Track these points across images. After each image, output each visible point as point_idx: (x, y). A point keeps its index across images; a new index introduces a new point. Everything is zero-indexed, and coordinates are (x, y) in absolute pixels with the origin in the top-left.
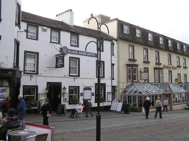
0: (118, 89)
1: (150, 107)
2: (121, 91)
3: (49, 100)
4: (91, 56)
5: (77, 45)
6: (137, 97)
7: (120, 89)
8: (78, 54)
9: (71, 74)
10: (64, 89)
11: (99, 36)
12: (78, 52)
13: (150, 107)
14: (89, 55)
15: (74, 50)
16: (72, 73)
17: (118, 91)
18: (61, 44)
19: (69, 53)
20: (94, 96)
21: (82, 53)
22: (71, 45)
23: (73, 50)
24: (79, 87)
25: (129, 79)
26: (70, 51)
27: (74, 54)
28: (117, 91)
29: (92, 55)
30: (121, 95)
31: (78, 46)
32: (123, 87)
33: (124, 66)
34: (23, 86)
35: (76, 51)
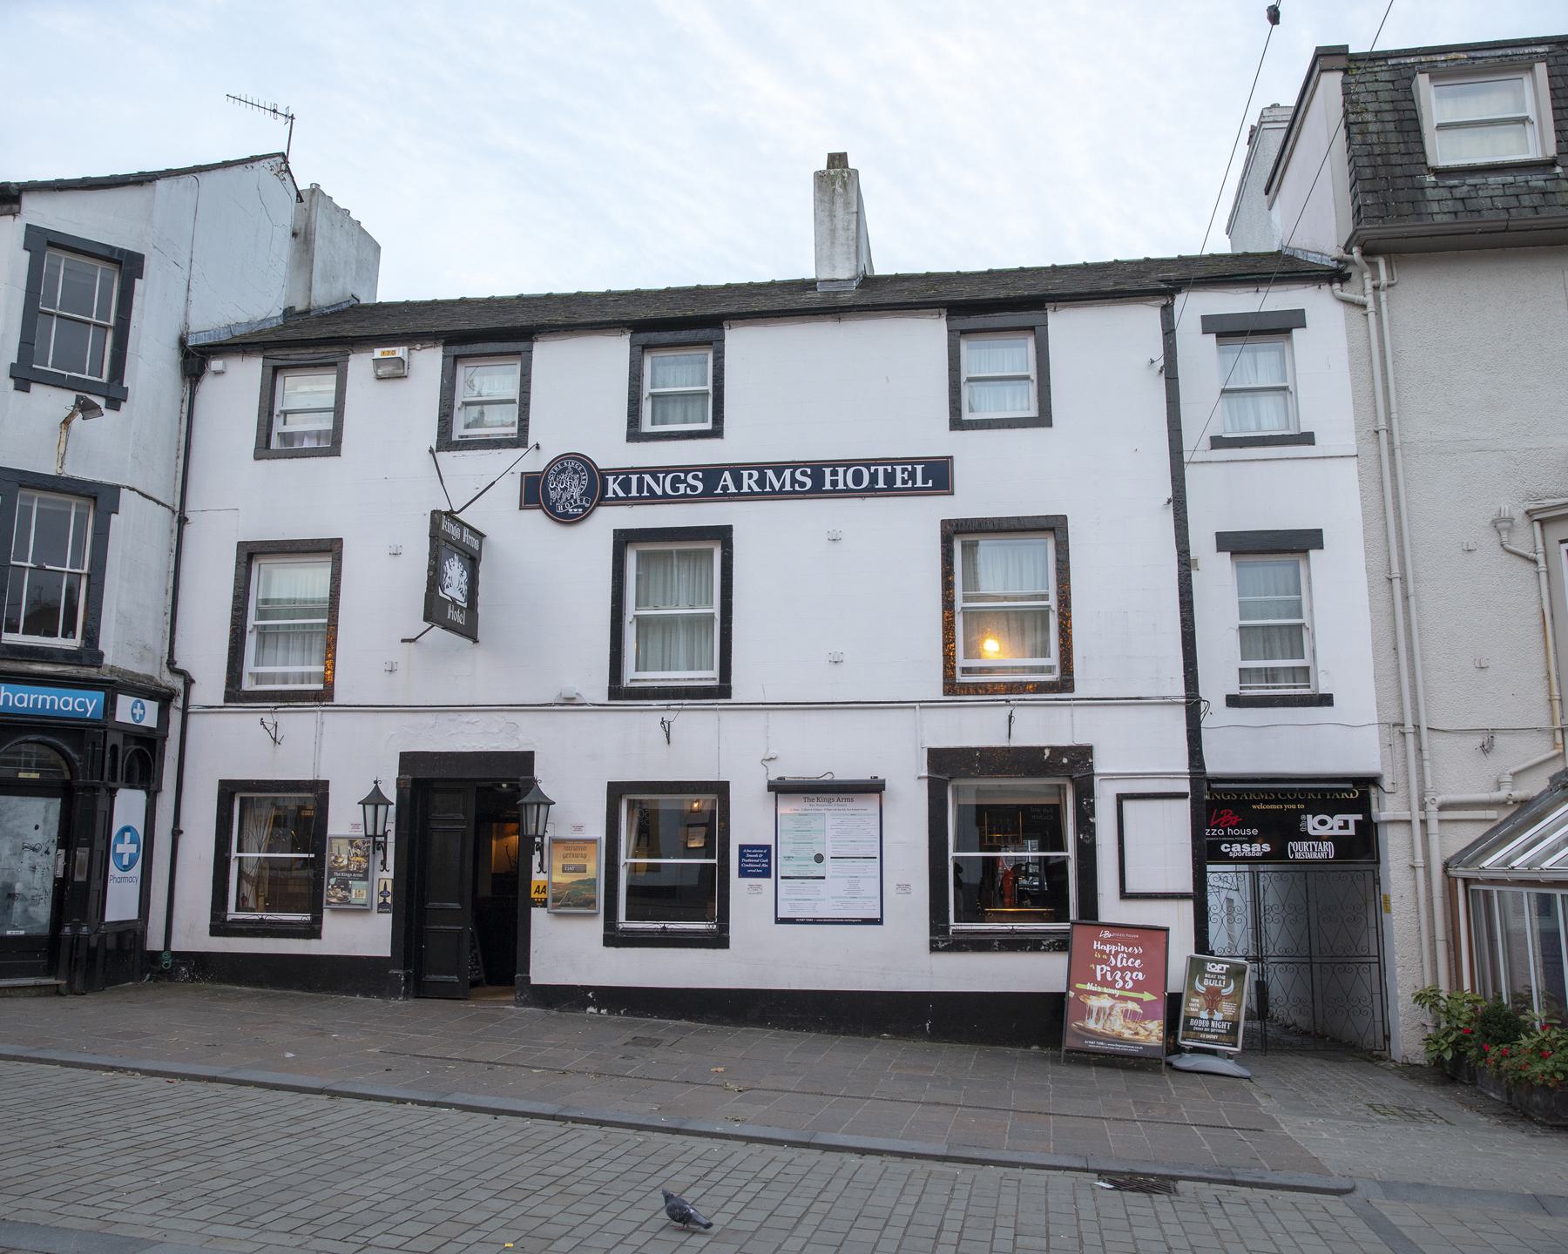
1: (1357, 822)
3: (147, 973)
4: (872, 491)
6: (50, 363)
8: (709, 495)
10: (370, 809)
11: (1271, 959)
12: (712, 484)
13: (1357, 822)
14: (845, 478)
15: (667, 470)
19: (617, 501)
23: (654, 472)
24: (319, 789)
26: (625, 485)
27: (665, 499)
32: (763, 1150)
35: (687, 470)
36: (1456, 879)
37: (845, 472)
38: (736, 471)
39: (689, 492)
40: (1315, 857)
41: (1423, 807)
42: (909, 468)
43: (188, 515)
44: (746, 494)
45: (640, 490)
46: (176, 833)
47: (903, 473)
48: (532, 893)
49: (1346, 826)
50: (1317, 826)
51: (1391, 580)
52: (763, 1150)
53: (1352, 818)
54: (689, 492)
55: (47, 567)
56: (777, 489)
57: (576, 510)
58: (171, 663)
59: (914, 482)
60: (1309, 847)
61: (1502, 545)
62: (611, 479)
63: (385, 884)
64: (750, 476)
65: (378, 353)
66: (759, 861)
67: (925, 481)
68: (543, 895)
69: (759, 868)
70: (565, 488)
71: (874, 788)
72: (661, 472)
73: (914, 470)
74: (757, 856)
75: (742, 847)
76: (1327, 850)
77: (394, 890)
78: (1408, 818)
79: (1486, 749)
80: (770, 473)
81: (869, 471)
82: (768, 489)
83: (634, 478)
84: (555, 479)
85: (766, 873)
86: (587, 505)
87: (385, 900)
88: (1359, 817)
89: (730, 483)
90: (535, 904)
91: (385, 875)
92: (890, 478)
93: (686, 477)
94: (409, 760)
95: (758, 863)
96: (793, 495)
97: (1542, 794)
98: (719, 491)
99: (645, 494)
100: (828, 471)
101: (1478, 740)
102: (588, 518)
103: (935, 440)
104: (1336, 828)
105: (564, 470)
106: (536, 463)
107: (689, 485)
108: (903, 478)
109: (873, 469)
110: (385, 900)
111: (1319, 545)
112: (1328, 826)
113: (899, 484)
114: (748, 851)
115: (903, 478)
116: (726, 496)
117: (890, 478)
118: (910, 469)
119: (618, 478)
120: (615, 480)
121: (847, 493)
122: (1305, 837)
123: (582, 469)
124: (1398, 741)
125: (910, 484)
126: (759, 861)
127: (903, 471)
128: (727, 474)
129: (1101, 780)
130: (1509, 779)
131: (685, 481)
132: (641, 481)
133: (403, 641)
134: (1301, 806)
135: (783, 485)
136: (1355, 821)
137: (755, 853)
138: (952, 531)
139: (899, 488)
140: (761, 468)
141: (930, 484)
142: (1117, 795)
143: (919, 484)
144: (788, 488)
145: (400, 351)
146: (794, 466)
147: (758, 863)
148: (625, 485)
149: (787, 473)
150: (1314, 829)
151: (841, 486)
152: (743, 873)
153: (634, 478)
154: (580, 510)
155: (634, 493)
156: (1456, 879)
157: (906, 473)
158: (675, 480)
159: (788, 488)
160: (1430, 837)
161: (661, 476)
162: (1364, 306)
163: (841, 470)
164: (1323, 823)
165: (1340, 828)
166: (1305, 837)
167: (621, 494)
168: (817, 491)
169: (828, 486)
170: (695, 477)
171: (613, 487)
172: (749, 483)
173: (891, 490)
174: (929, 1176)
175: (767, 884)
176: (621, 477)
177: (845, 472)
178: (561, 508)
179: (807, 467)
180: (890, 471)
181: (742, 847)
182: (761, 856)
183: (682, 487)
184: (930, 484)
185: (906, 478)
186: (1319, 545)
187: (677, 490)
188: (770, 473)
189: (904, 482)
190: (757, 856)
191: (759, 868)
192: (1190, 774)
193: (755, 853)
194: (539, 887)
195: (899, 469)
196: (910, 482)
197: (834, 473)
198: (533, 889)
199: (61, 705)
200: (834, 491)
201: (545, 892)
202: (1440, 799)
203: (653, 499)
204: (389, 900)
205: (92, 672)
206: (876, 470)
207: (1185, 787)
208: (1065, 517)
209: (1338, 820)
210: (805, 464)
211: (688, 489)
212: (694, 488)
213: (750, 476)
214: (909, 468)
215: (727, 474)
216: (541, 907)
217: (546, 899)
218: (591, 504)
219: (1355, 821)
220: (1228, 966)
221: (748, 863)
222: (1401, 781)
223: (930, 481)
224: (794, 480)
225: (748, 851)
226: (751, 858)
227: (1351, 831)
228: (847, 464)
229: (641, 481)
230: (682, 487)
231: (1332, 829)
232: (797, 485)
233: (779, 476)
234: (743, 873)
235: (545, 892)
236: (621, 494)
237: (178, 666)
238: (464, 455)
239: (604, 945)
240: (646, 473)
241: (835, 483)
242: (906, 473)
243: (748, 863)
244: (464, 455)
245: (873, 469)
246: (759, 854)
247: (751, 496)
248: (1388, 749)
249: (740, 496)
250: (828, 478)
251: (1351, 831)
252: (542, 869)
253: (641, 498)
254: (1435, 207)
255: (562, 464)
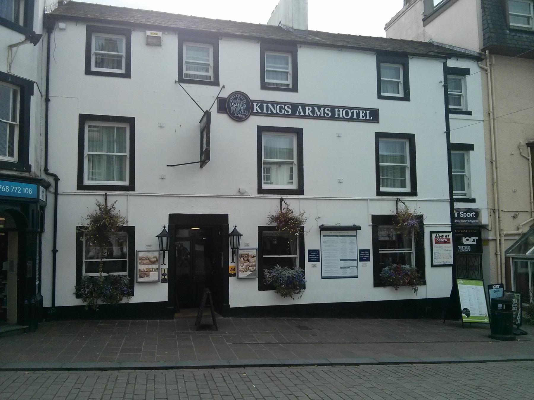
0: (490, 238)
2: (506, 245)
4: (351, 119)
5: (289, 82)
7: (503, 238)
8: (293, 115)
9: (383, 189)
14: (343, 114)
15: (278, 103)
16: (457, 190)
17: (492, 245)
18: (221, 85)
19: (257, 114)
20: (368, 260)
21: (313, 111)
22: (264, 86)
23: (272, 103)
25: (266, 181)
26: (261, 107)
27: (277, 115)
28: (488, 245)
29: (352, 114)
30: (507, 259)
31: (295, 89)
33: (516, 153)
34: (308, 250)
35: (285, 104)
36: (510, 258)
37: (343, 111)
38: (304, 106)
39: (286, 113)
40: (465, 251)
41: (500, 235)
42: (364, 111)
43: (50, 98)
44: (307, 116)
45: (267, 110)
46: (55, 251)
47: (362, 113)
48: (230, 270)
49: (474, 241)
50: (466, 241)
51: (492, 162)
52: (95, 374)
53: (476, 238)
54: (286, 113)
55: (2, 120)
56: (319, 115)
57: (242, 116)
58: (46, 170)
59: (366, 117)
60: (463, 248)
61: (520, 154)
62: (255, 104)
63: (164, 270)
64: (309, 109)
65: (149, 33)
66: (315, 256)
67: (370, 117)
68: (234, 272)
69: (315, 258)
70: (237, 106)
71: (356, 228)
72: (275, 104)
73: (366, 112)
74: (314, 254)
75: (309, 251)
76: (468, 249)
77: (168, 272)
78: (496, 239)
79: (514, 217)
80: (316, 109)
81: (351, 111)
82: (315, 115)
83: (265, 105)
84: (233, 102)
85: (318, 260)
86: (247, 114)
87: (164, 277)
88: (477, 238)
89: (301, 111)
90: (231, 275)
91: (164, 266)
92: (358, 115)
93: (285, 107)
94: (172, 217)
95: (315, 257)
96: (324, 118)
97: (527, 232)
98: (297, 114)
99: (269, 112)
100: (336, 110)
101: (512, 214)
102: (248, 119)
103: (374, 103)
104: (471, 242)
105: (236, 98)
106: (225, 94)
107: (286, 110)
108: (362, 115)
109: (352, 111)
110: (164, 277)
111: (473, 149)
112: (469, 241)
113: (361, 118)
114: (311, 252)
115: (362, 115)
116: (300, 117)
117: (358, 115)
118: (365, 112)
119: (258, 104)
120: (257, 105)
121: (343, 119)
122: (462, 244)
123: (244, 99)
124: (492, 214)
125: (365, 118)
126: (315, 256)
127: (363, 112)
128: (300, 107)
129: (426, 226)
130: (521, 227)
131: (284, 108)
132: (267, 106)
133: (168, 166)
134: (461, 235)
135: (321, 114)
136: (476, 239)
137: (314, 253)
138: (379, 136)
139: (361, 119)
140: (313, 106)
141: (371, 119)
142: (430, 232)
143: (368, 118)
144: (322, 115)
145: (160, 34)
146: (325, 107)
147: (315, 257)
148: (261, 107)
149: (322, 109)
150: (465, 242)
151: (341, 116)
152: (310, 260)
153: (265, 105)
154: (244, 116)
155: (265, 111)
156: (510, 258)
157: (363, 113)
158: (281, 108)
159: (322, 115)
160: (502, 245)
161: (275, 105)
162: (487, 71)
163: (341, 110)
164: (467, 240)
165: (472, 242)
166: (462, 244)
167: (260, 111)
168: (332, 118)
169: (337, 116)
170: (288, 107)
171: (256, 108)
172: (308, 112)
173: (358, 120)
174: (155, 377)
175: (318, 264)
176: (259, 104)
177: (343, 111)
178: (236, 114)
179: (330, 108)
180: (358, 112)
181: (309, 251)
182: (316, 254)
183: (283, 111)
184: (371, 119)
185: (363, 116)
186: (473, 149)
187: (282, 112)
188: (316, 109)
189: (363, 117)
190: (314, 254)
191: (315, 258)
192: (451, 225)
193: (314, 253)
194: (232, 268)
195: (361, 111)
196: (365, 117)
197: (339, 111)
198: (230, 269)
199: (6, 190)
200: (339, 118)
201: (235, 270)
202: (505, 232)
203: (272, 115)
204: (166, 277)
205: (27, 175)
206: (353, 111)
207: (449, 229)
208: (414, 135)
209: (471, 239)
210: (328, 106)
211: (286, 112)
212: (288, 112)
213: (309, 109)
214: (364, 111)
215: (300, 107)
216: (233, 276)
217: (235, 273)
218: (248, 114)
219: (476, 239)
220: (499, 285)
221: (311, 257)
222: (493, 227)
223: (372, 117)
224: (324, 113)
225: (311, 252)
226: (312, 255)
227: (475, 243)
228: (344, 108)
229: (267, 106)
230: (283, 111)
231: (470, 242)
232: (325, 114)
233: (319, 110)
234: (310, 260)
235: (235, 270)
236: (260, 111)
237: (51, 171)
238: (191, 86)
239: (259, 290)
240: (269, 103)
241: (339, 115)
242: (363, 113)
243: (311, 257)
244: (191, 86)
245: (352, 111)
246: (315, 253)
247: (309, 117)
248: (490, 217)
249: (305, 117)
250: (337, 113)
251: (475, 243)
252: (233, 261)
253: (267, 113)
254: (509, 42)
255: (235, 96)
